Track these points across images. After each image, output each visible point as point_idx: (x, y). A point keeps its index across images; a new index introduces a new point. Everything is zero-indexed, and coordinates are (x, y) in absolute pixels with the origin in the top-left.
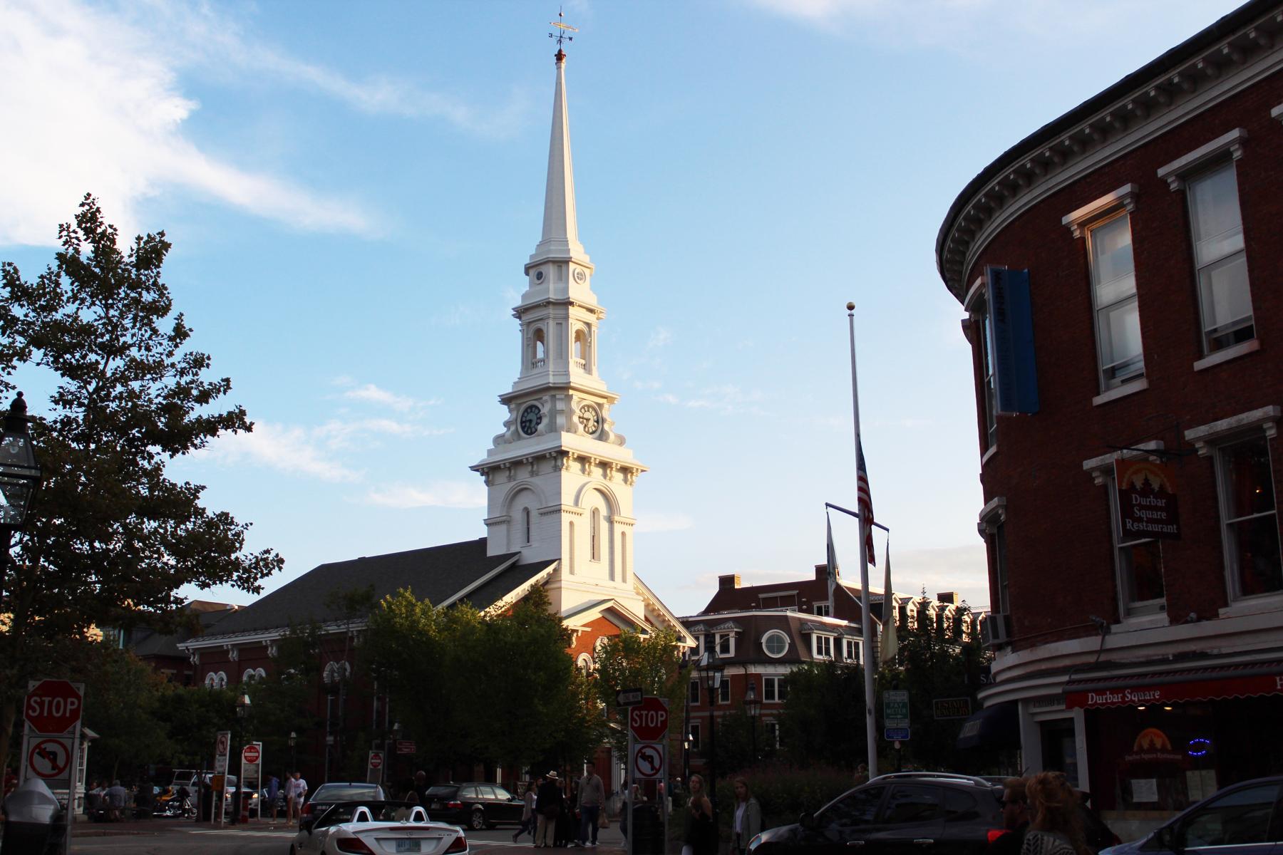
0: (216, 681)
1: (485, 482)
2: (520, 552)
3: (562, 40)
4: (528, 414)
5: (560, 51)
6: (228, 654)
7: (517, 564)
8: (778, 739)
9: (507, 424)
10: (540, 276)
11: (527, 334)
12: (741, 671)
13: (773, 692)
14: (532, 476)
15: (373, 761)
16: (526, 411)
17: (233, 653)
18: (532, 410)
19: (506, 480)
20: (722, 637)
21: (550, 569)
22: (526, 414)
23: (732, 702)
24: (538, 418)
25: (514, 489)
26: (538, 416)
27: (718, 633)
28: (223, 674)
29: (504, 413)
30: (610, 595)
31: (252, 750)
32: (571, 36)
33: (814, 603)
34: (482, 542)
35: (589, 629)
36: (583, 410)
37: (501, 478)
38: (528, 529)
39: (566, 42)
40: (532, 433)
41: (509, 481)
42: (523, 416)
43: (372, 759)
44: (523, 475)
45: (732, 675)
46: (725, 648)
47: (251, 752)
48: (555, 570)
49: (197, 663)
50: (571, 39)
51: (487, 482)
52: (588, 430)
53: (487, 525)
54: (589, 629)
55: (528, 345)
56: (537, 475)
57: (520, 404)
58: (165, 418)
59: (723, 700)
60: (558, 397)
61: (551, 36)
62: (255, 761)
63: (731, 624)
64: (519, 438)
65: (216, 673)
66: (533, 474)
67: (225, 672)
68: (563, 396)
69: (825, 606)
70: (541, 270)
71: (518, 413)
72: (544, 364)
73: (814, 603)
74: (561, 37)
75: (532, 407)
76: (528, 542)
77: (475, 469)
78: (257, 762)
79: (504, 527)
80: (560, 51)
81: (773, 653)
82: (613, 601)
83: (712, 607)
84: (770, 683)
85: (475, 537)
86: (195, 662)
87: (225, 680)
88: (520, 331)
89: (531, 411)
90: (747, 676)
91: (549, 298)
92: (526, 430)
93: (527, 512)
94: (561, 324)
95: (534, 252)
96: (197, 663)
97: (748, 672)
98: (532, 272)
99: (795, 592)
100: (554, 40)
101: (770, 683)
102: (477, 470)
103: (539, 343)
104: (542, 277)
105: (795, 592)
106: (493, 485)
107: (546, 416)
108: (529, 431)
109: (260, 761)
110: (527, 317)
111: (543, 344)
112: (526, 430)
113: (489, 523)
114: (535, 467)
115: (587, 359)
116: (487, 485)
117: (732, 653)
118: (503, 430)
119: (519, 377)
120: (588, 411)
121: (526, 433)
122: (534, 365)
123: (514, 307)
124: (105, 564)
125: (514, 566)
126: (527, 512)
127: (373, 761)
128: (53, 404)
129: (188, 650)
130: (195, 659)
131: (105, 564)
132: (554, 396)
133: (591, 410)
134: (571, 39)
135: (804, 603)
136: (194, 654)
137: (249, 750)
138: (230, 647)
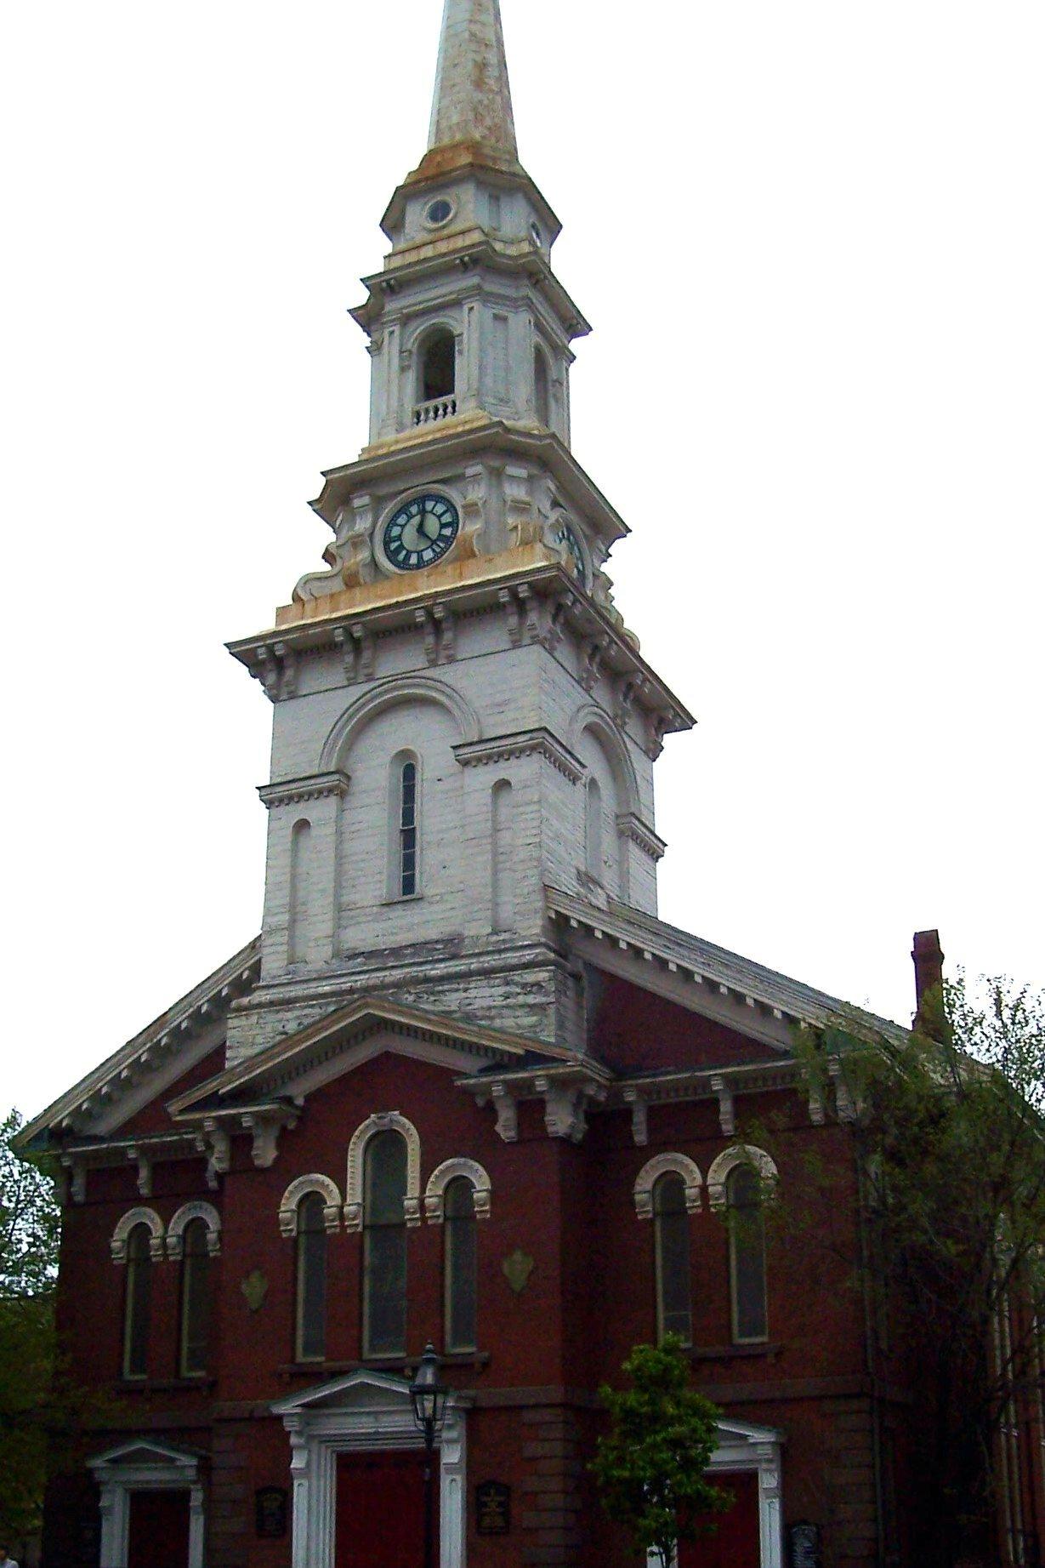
18: (420, 557)
42: (392, 522)
53: (269, 804)
70: (447, 199)
106: (293, 696)
108: (414, 560)
119: (366, 445)
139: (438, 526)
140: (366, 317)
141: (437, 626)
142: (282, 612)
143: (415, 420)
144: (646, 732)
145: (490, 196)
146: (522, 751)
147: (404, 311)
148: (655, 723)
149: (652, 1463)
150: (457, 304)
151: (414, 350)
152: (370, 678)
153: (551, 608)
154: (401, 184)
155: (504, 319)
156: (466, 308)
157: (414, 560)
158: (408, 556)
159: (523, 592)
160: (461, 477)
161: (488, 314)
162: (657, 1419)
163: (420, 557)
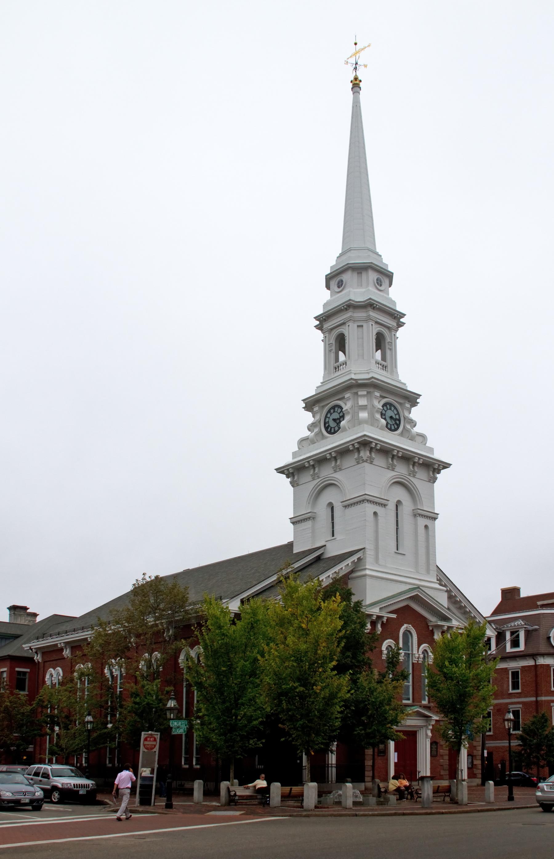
0: (55, 676)
1: (291, 483)
2: (325, 546)
3: (357, 66)
4: (331, 414)
5: (356, 79)
6: (63, 652)
7: (322, 558)
9: (310, 428)
10: (340, 284)
11: (329, 340)
12: (531, 663)
14: (335, 471)
16: (329, 411)
17: (66, 651)
18: (334, 430)
19: (310, 478)
20: (512, 633)
21: (355, 558)
22: (329, 415)
23: (522, 690)
25: (319, 485)
27: (508, 630)
28: (59, 669)
29: (309, 418)
32: (366, 64)
34: (290, 545)
35: (394, 616)
36: (385, 408)
37: (306, 477)
38: (333, 523)
41: (314, 479)
42: (326, 417)
44: (326, 472)
45: (522, 667)
46: (515, 643)
48: (359, 559)
49: (40, 660)
51: (293, 484)
52: (391, 427)
53: (293, 523)
54: (394, 616)
55: (330, 351)
56: (341, 469)
57: (323, 407)
59: (514, 688)
60: (360, 393)
62: (153, 748)
63: (521, 622)
64: (323, 437)
65: (54, 669)
66: (337, 469)
67: (61, 667)
68: (365, 393)
70: (341, 278)
71: (321, 416)
72: (345, 367)
74: (356, 64)
75: (334, 408)
76: (333, 536)
77: (280, 470)
78: (154, 750)
79: (308, 524)
80: (356, 79)
83: (496, 612)
85: (285, 542)
86: (38, 660)
87: (62, 675)
88: (322, 340)
89: (334, 412)
90: (536, 666)
91: (350, 300)
92: (329, 430)
93: (331, 507)
94: (362, 326)
95: (334, 263)
96: (40, 660)
97: (537, 664)
98: (334, 284)
100: (351, 68)
102: (282, 472)
103: (341, 353)
104: (342, 285)
106: (298, 485)
107: (348, 413)
108: (333, 431)
109: (157, 749)
110: (328, 325)
111: (345, 353)
112: (329, 430)
113: (295, 521)
114: (339, 462)
115: (318, 812)
116: (293, 486)
117: (522, 647)
118: (307, 433)
119: (322, 381)
120: (390, 409)
121: (330, 433)
122: (336, 368)
123: (315, 316)
125: (319, 559)
126: (331, 507)
129: (31, 649)
130: (38, 658)
132: (356, 393)
133: (393, 408)
136: (36, 653)
138: (63, 645)
139: (330, 425)
140: (319, 327)
141: (335, 459)
142: (294, 454)
143: (335, 371)
144: (429, 474)
145: (358, 273)
146: (351, 505)
147: (329, 328)
148: (432, 470)
149: (88, 647)
150: (344, 324)
151: (334, 343)
152: (319, 477)
153: (368, 448)
154: (340, 252)
155: (362, 326)
156: (347, 325)
157: (333, 431)
158: (331, 430)
159: (357, 446)
160: (343, 398)
161: (355, 325)
162: (232, 675)
163: (334, 430)
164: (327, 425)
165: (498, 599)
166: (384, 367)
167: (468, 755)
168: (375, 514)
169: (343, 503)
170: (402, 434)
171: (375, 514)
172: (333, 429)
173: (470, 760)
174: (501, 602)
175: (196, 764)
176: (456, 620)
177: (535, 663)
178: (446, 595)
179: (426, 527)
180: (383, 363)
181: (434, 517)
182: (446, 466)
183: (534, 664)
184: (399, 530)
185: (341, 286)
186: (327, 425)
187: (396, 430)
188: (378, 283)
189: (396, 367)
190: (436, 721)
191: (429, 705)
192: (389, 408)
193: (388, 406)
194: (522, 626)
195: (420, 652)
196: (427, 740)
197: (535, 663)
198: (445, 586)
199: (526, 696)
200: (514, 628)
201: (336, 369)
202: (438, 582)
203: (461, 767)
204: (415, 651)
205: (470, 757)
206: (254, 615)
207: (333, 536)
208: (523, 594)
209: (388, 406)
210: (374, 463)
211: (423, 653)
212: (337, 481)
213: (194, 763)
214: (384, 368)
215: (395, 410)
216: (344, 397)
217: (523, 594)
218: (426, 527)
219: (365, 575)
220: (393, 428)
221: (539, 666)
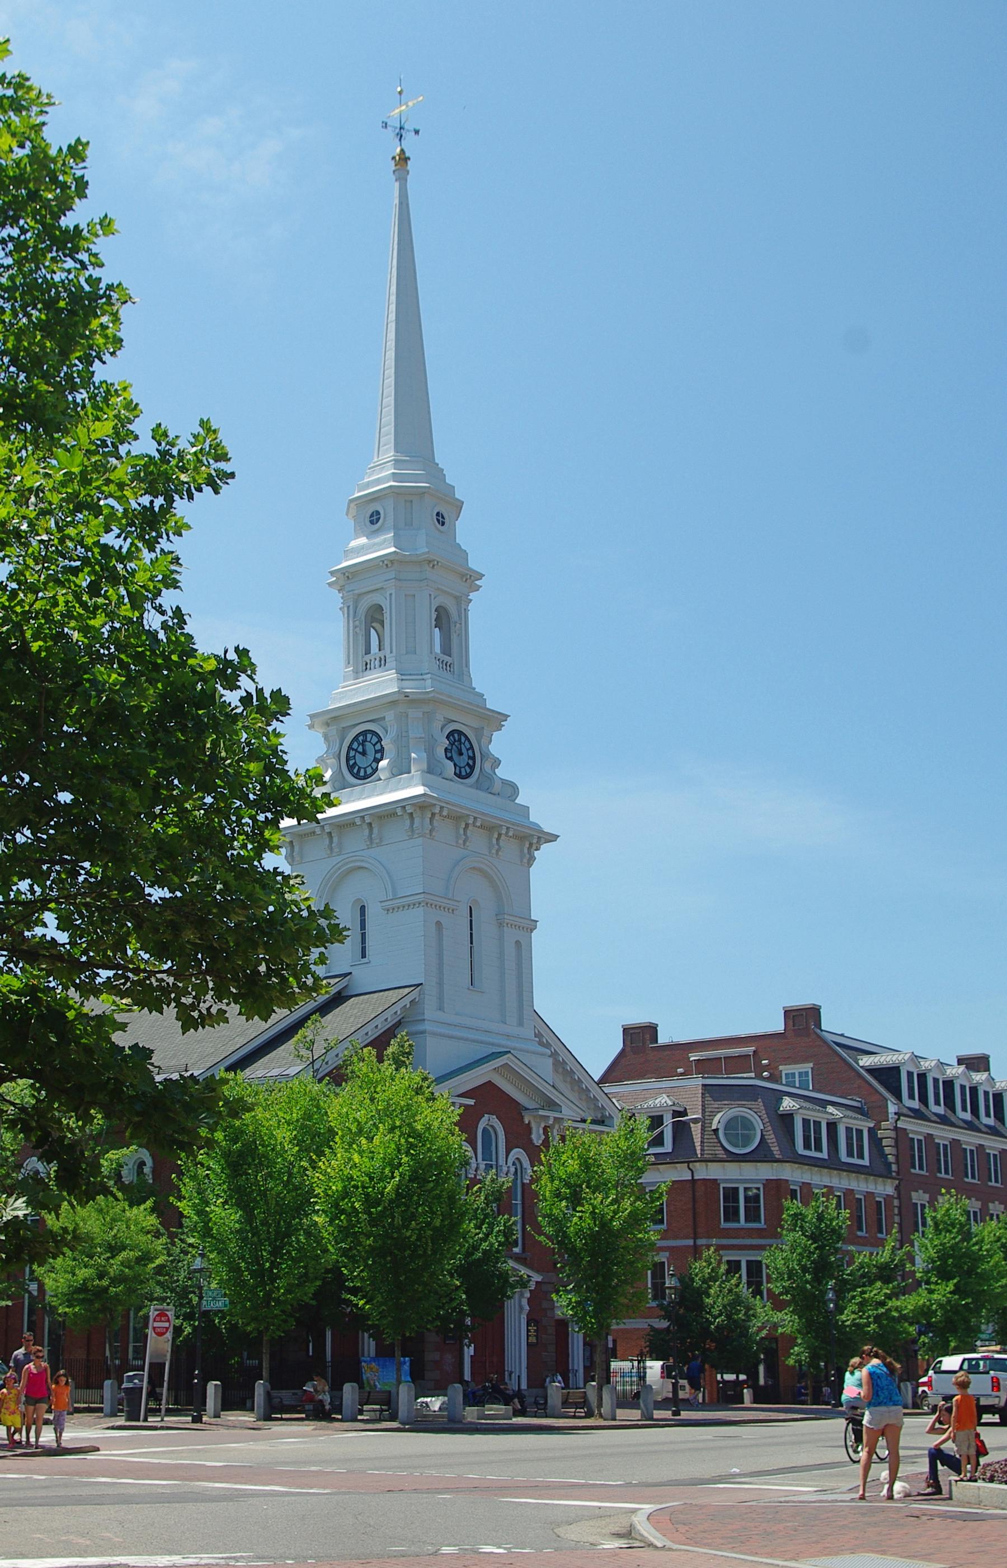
2: (351, 973)
7: (343, 994)
8: (650, 1291)
13: (736, 1210)
15: (156, 1324)
18: (365, 772)
24: (376, 752)
26: (378, 747)
30: (493, 1044)
31: (163, 1319)
32: (417, 128)
33: (781, 1068)
39: (409, 137)
40: (366, 777)
43: (154, 1320)
47: (161, 1321)
50: (417, 132)
52: (460, 772)
58: (39, 651)
61: (385, 125)
69: (800, 1074)
73: (781, 1068)
76: (364, 956)
81: (735, 1146)
82: (509, 1055)
84: (732, 1194)
90: (693, 1181)
92: (355, 771)
97: (696, 1178)
99: (750, 1050)
100: (390, 134)
101: (732, 1194)
105: (750, 1050)
108: (362, 773)
112: (355, 771)
121: (357, 776)
124: (157, 894)
127: (156, 1324)
128: (191, 436)
131: (157, 894)
134: (417, 132)
135: (766, 1068)
137: (158, 1319)
163: (365, 772)
164: (351, 762)
165: (616, 1045)
166: (447, 666)
167: (585, 1344)
168: (439, 924)
169: (383, 904)
170: (478, 785)
171: (439, 924)
172: (362, 771)
173: (588, 1354)
174: (623, 1051)
175: (134, 1359)
176: (568, 1107)
177: (693, 1176)
178: (551, 1061)
179: (518, 943)
180: (446, 658)
181: (532, 925)
182: (553, 838)
183: (690, 1178)
184: (475, 949)
185: (377, 523)
186: (351, 762)
187: (468, 776)
188: (438, 520)
189: (467, 665)
190: (537, 1282)
191: (524, 1256)
192: (457, 739)
193: (456, 735)
194: (668, 1108)
195: (510, 1163)
196: (522, 1316)
197: (693, 1176)
198: (547, 1045)
199: (676, 1237)
200: (653, 1110)
201: (366, 664)
202: (537, 1039)
203: (573, 1366)
204: (502, 1161)
205: (588, 1348)
206: (887, 1281)
207: (364, 956)
208: (663, 1039)
209: (456, 735)
210: (435, 838)
211: (514, 1164)
212: (367, 862)
213: (130, 1356)
214: (448, 668)
215: (467, 742)
216: (384, 717)
217: (663, 1039)
218: (518, 943)
219: (423, 1032)
220: (463, 773)
221: (699, 1182)
